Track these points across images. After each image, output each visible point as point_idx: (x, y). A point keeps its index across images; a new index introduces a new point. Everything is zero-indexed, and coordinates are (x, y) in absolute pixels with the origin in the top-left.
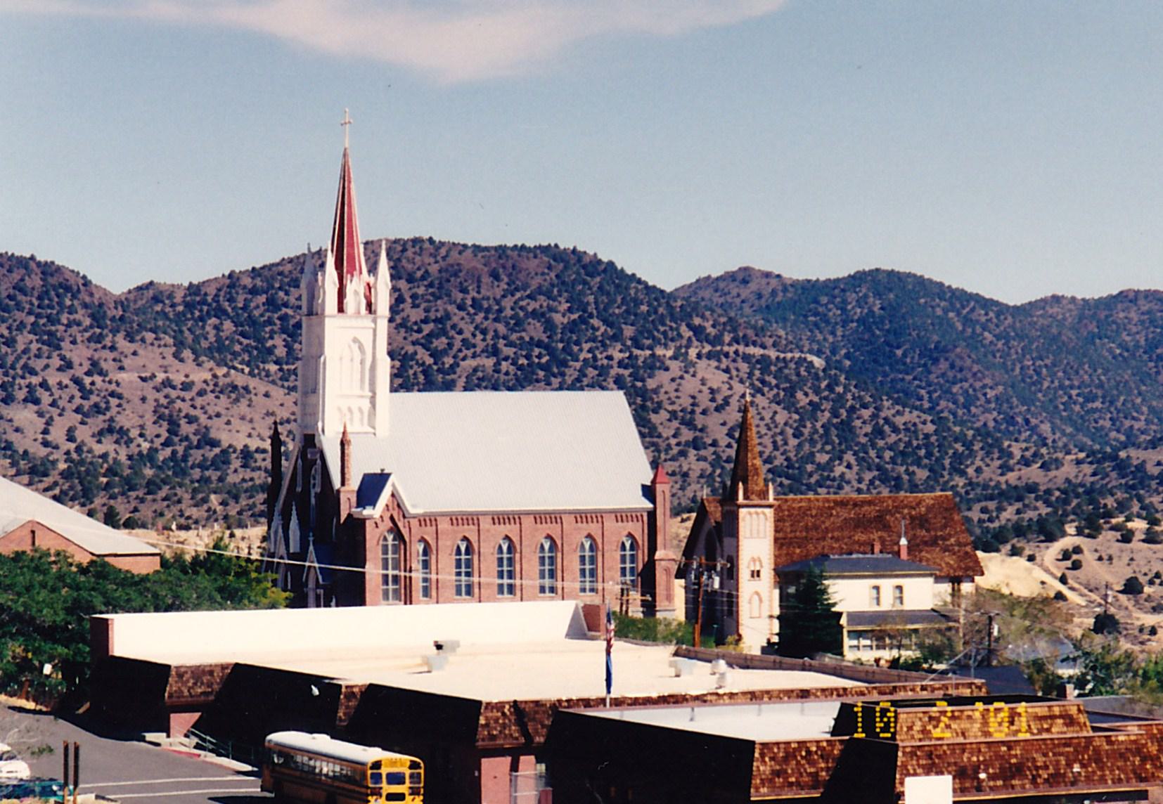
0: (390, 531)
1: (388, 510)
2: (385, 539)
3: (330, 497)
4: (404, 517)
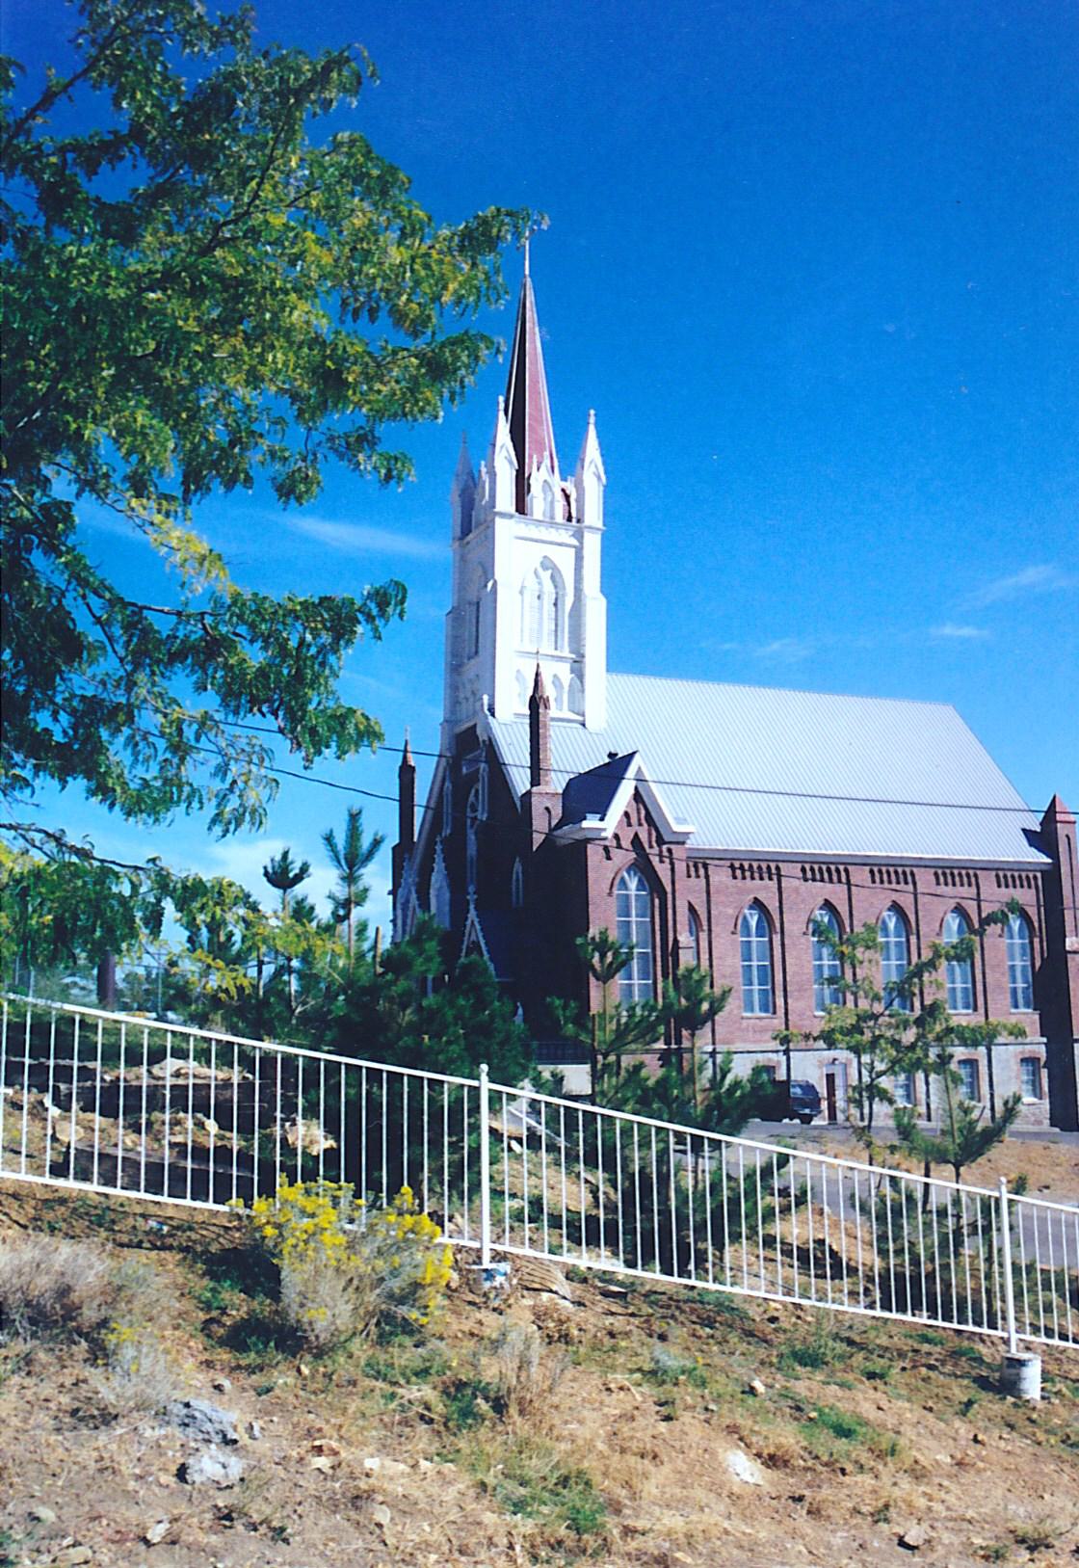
0: (633, 867)
1: (629, 825)
2: (624, 884)
3: (514, 812)
4: (660, 841)
